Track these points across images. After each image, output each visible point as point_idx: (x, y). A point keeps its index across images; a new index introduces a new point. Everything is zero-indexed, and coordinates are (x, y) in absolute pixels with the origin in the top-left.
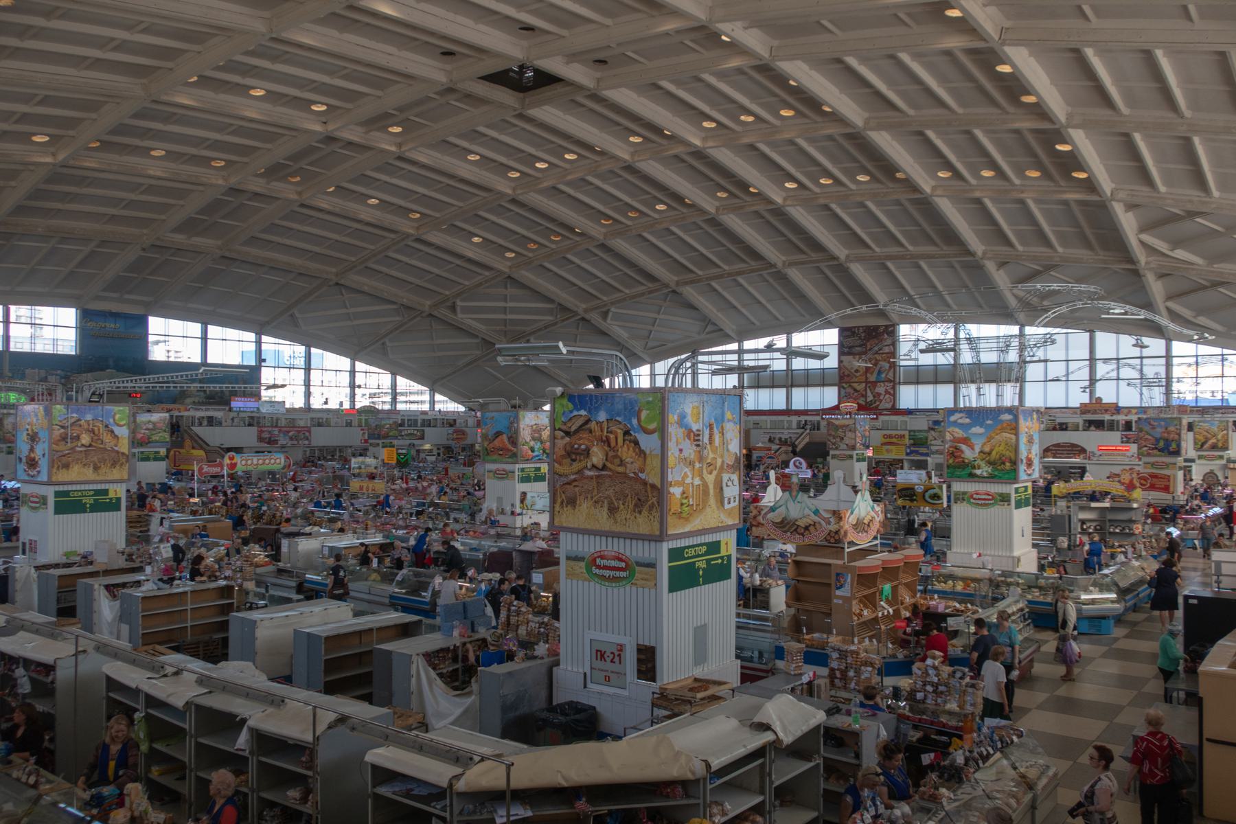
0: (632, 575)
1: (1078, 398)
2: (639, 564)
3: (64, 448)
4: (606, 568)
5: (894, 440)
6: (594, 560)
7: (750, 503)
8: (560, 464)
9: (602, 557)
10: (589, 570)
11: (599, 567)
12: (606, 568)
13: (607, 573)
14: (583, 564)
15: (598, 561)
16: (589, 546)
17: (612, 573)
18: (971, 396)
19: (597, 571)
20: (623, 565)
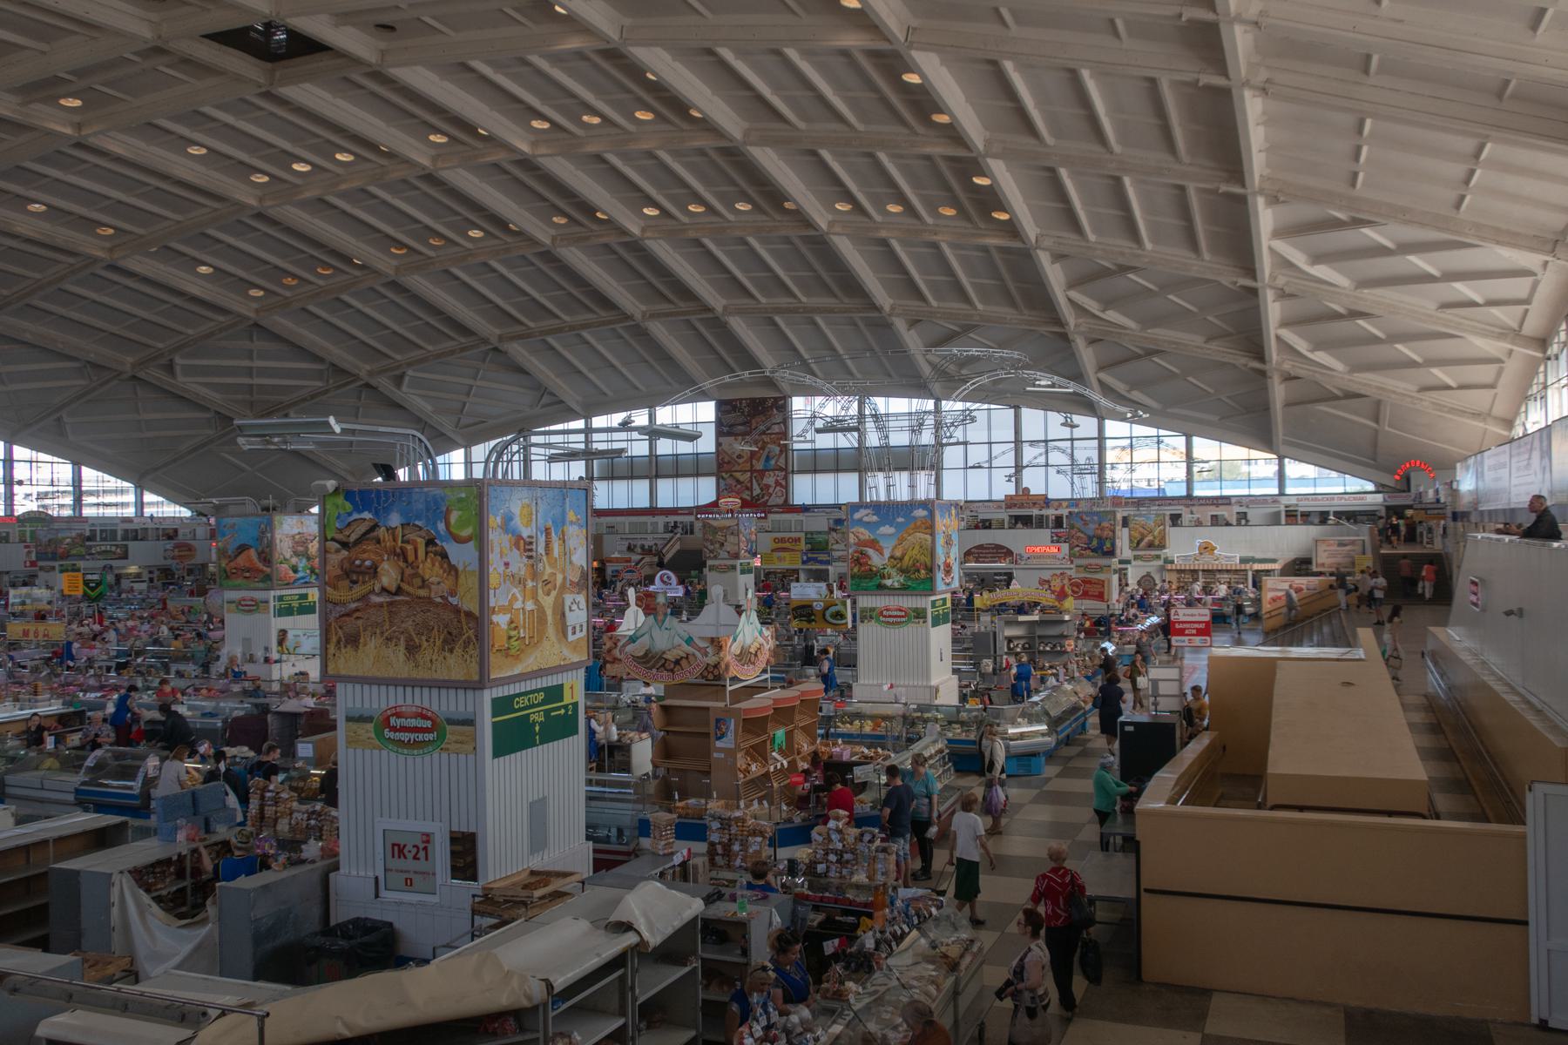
0: (442, 737)
2: (451, 722)
4: (404, 729)
5: (787, 545)
6: (387, 719)
9: (398, 715)
10: (380, 734)
11: (394, 729)
12: (404, 729)
13: (405, 736)
15: (392, 720)
17: (412, 736)
19: (392, 735)
20: (428, 724)
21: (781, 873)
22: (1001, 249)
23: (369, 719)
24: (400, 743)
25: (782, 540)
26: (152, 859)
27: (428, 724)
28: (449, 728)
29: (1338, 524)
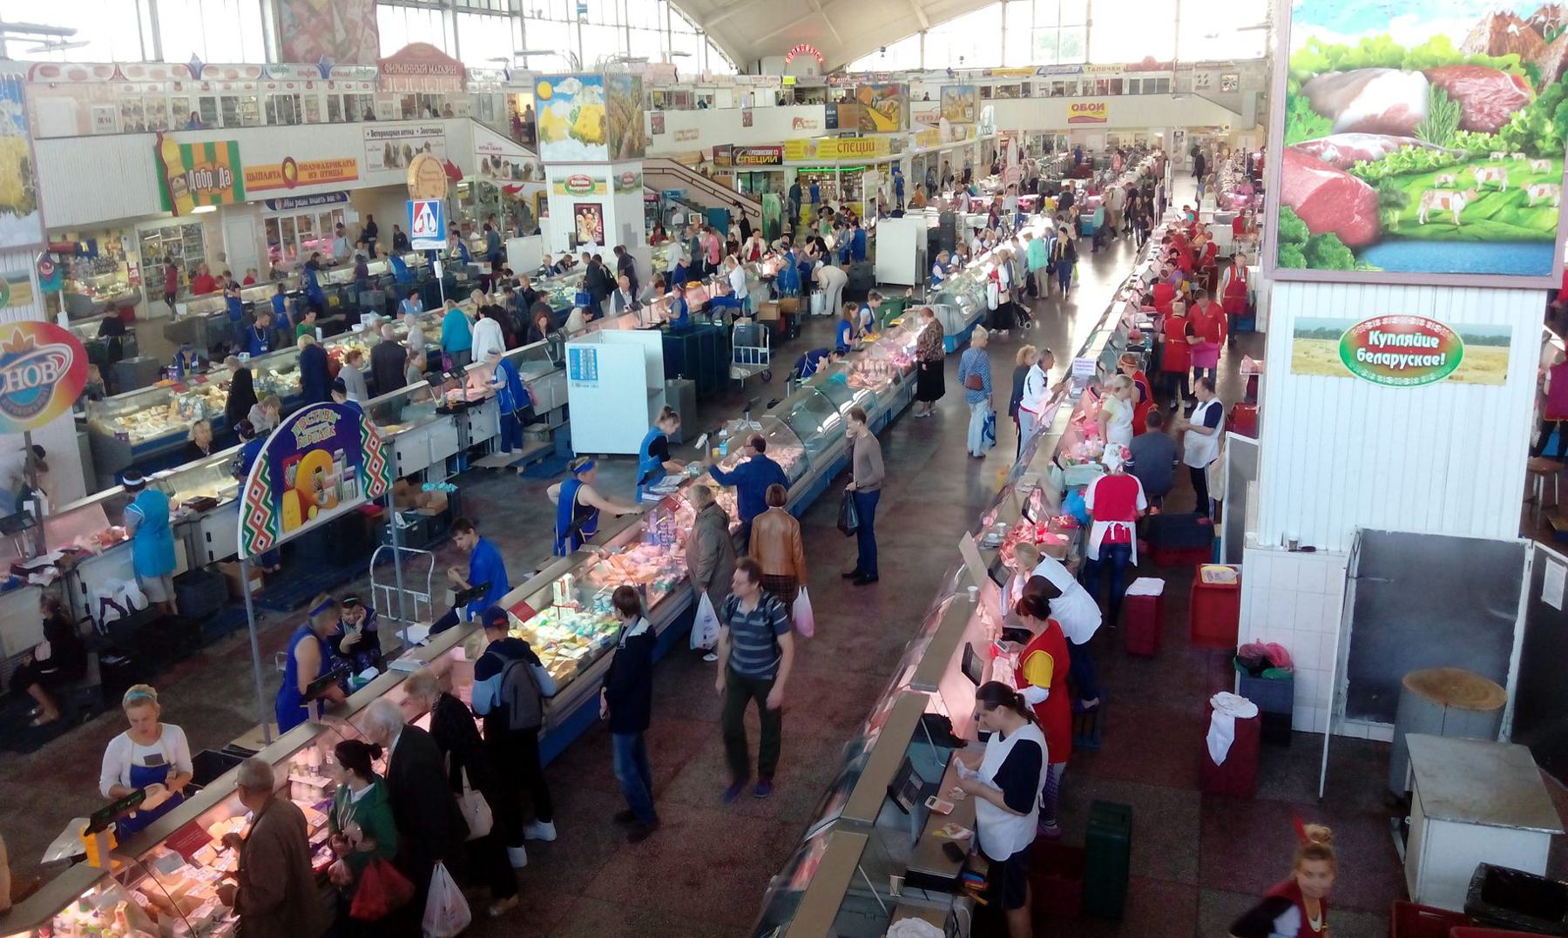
0: (1453, 361)
1: (1081, 60)
2: (1471, 340)
3: (1028, 623)
4: (1389, 349)
5: (1088, 113)
6: (1364, 336)
7: (1549, 156)
8: (1157, 159)
9: (1383, 329)
10: (1347, 355)
11: (1375, 349)
12: (1389, 349)
13: (1391, 359)
14: (1334, 345)
15: (1373, 338)
16: (566, 173)
17: (1403, 359)
18: (907, 177)
19: (1369, 357)
20: (1434, 342)
21: (309, 20)
22: (257, 627)
23: (1335, 334)
24: (1383, 368)
25: (1083, 107)
26: (44, 890)
27: (1434, 342)
28: (1466, 348)
29: (654, 270)
